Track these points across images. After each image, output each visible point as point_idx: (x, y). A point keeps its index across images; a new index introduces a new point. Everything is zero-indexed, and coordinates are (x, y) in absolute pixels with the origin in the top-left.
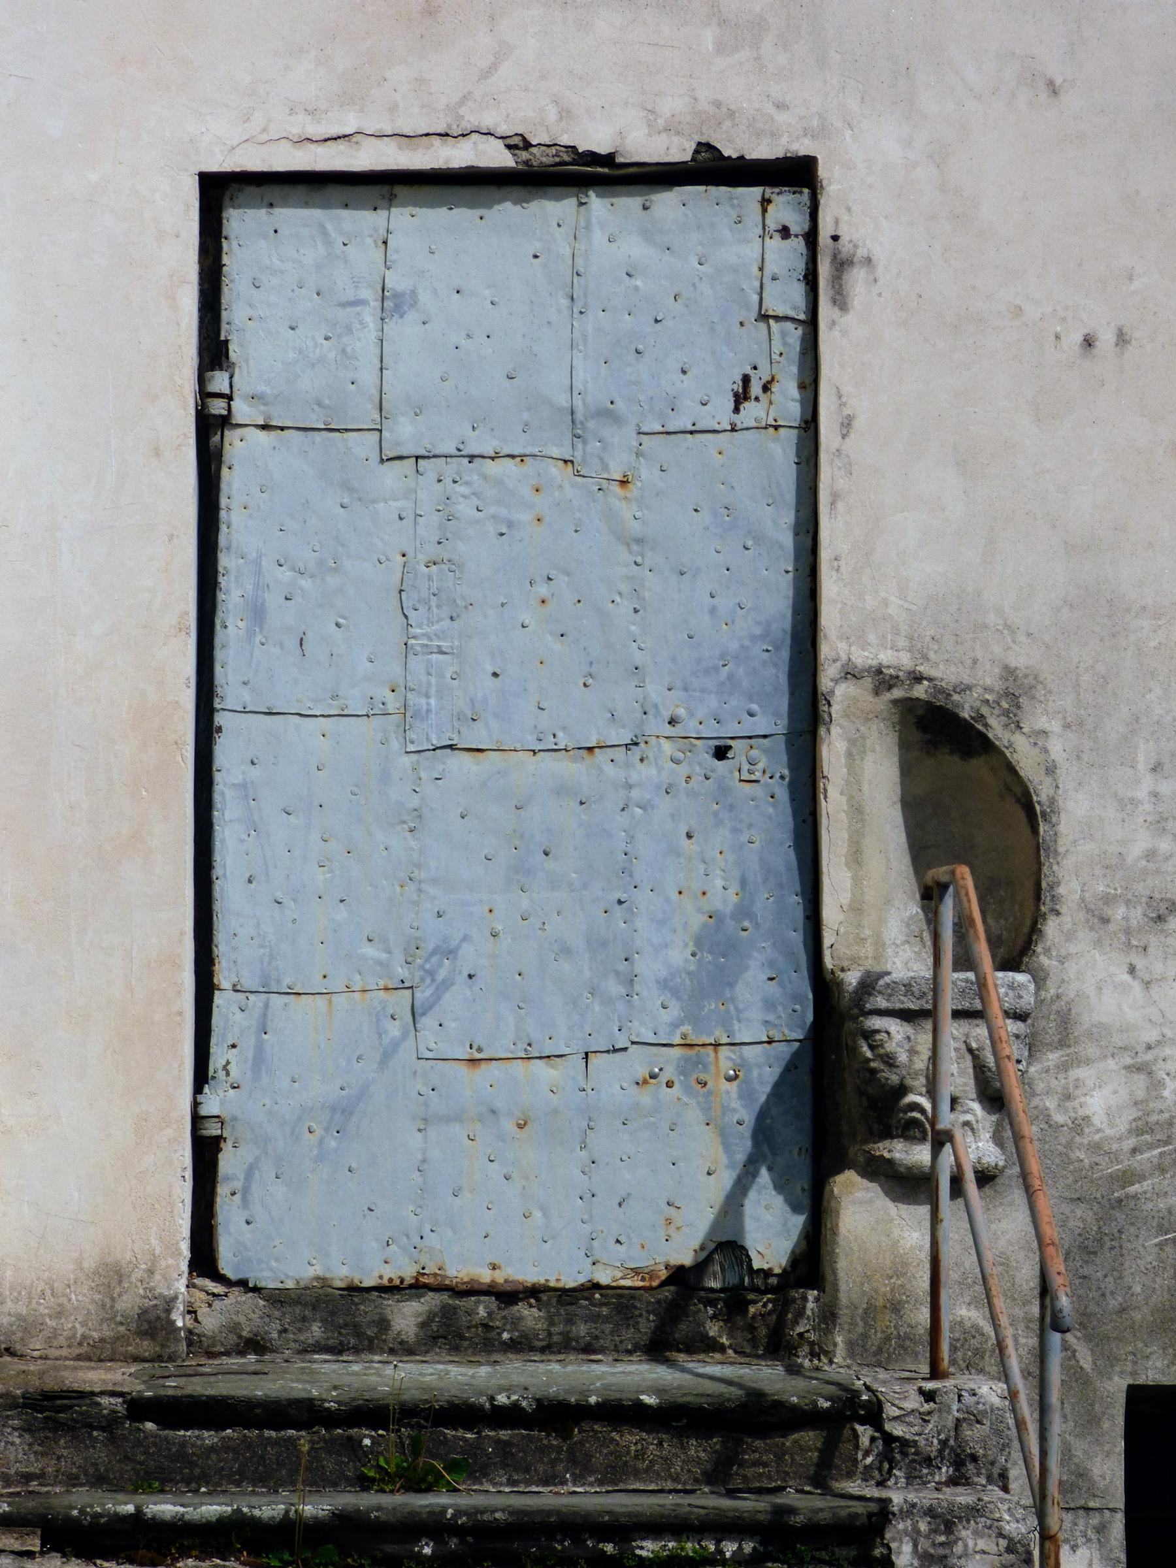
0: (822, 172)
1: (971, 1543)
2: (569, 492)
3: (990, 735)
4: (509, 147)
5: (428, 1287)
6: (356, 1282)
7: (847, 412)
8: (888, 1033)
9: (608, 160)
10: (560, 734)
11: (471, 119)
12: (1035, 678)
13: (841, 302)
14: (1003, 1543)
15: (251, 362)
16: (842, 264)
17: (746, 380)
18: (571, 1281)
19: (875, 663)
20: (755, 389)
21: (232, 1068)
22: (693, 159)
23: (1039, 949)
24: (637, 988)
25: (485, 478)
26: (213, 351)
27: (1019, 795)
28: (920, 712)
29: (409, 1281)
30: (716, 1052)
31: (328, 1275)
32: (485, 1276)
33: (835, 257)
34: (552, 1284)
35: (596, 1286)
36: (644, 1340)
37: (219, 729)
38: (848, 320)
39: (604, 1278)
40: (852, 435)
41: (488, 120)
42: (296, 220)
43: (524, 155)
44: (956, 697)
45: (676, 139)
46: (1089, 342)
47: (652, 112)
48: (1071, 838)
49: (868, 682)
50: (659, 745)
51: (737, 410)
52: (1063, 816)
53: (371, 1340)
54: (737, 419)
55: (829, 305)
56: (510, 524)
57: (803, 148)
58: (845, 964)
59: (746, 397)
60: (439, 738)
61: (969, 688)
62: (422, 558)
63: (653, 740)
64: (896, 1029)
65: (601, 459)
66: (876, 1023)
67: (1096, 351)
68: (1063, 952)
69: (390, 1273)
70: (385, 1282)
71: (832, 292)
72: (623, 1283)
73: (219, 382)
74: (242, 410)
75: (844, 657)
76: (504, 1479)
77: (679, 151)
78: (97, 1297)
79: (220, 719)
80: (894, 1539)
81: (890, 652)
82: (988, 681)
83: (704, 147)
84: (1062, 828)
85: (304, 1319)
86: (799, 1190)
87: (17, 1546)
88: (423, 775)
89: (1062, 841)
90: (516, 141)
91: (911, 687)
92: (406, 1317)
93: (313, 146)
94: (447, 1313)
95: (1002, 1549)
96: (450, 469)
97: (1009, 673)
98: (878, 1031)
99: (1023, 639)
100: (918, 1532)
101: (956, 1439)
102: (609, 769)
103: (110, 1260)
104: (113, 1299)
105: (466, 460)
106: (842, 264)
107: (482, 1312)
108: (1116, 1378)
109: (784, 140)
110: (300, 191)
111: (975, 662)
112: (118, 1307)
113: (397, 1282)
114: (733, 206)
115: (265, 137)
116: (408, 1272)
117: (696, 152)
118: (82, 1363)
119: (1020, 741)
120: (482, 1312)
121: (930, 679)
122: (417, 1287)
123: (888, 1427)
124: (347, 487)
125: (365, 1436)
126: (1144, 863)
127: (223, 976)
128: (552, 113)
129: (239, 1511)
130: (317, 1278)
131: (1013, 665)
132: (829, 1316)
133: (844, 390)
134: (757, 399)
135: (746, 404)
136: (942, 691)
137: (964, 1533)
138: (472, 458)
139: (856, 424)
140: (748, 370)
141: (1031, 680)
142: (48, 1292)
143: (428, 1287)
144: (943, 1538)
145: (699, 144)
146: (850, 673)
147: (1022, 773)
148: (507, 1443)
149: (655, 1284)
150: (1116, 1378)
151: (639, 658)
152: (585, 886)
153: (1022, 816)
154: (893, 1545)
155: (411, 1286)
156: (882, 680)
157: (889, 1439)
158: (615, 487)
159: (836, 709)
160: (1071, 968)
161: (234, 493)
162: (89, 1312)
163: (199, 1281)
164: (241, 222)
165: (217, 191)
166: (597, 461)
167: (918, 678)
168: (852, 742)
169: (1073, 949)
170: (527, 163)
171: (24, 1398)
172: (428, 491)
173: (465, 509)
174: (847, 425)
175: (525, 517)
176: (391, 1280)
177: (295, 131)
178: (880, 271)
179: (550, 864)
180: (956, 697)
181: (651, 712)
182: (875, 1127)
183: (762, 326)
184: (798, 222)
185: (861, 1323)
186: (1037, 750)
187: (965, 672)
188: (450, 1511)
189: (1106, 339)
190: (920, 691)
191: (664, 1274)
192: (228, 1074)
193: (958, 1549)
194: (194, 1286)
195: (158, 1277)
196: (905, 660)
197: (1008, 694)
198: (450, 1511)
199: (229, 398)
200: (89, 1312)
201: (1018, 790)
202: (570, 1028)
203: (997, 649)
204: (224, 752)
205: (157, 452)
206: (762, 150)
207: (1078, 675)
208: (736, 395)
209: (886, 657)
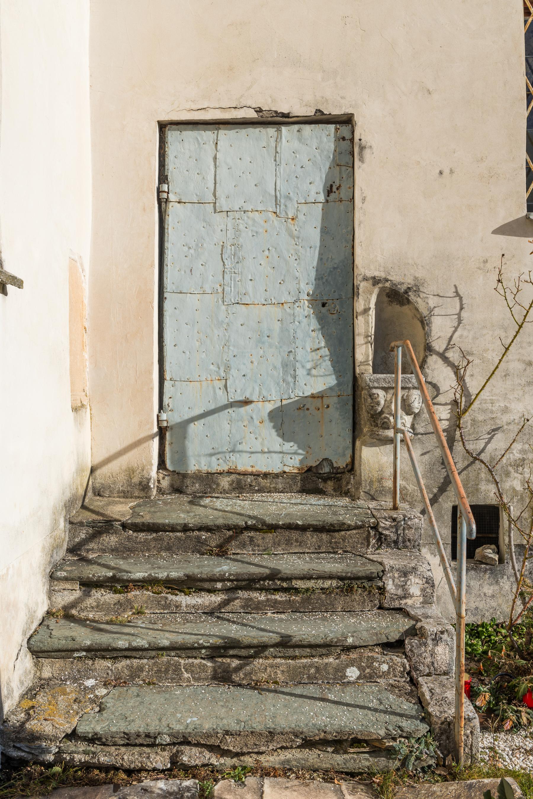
0: (356, 118)
1: (413, 581)
2: (276, 223)
3: (410, 298)
4: (256, 111)
5: (232, 473)
6: (210, 471)
7: (364, 195)
8: (378, 394)
9: (287, 116)
10: (273, 299)
11: (243, 103)
12: (424, 280)
13: (362, 160)
14: (425, 580)
15: (175, 182)
16: (362, 148)
17: (331, 186)
18: (276, 471)
19: (373, 275)
20: (334, 189)
21: (170, 405)
22: (315, 115)
23: (425, 367)
24: (297, 379)
25: (248, 217)
26: (163, 178)
27: (419, 317)
28: (388, 291)
29: (226, 471)
30: (322, 399)
31: (200, 469)
32: (250, 469)
33: (360, 146)
34: (271, 472)
35: (285, 472)
36: (298, 489)
37: (166, 298)
38: (364, 166)
39: (287, 469)
40: (366, 203)
41: (249, 104)
42: (189, 134)
43: (261, 114)
44: (399, 286)
45: (309, 108)
46: (441, 173)
47: (302, 100)
48: (435, 331)
49: (371, 282)
50: (304, 303)
51: (328, 196)
52: (433, 324)
53: (214, 489)
54: (328, 198)
55: (358, 161)
56: (257, 233)
57: (350, 111)
58: (363, 372)
59: (332, 192)
60: (234, 300)
61: (403, 283)
62: (229, 244)
63: (302, 301)
64: (381, 393)
65: (286, 212)
66: (375, 391)
67: (443, 175)
68: (433, 368)
69: (220, 469)
70: (218, 471)
71: (359, 157)
72: (293, 471)
73: (165, 187)
74: (172, 197)
75: (363, 274)
76: (250, 549)
77: (310, 112)
78: (126, 478)
79: (166, 295)
80: (386, 580)
81: (378, 272)
82: (409, 281)
83: (319, 111)
84: (433, 328)
85: (194, 483)
86: (348, 442)
87: (70, 588)
88: (229, 312)
89: (432, 332)
90: (258, 109)
91: (385, 283)
92: (225, 482)
93: (194, 112)
94: (239, 482)
95: (424, 582)
96: (237, 215)
97: (416, 279)
98: (375, 394)
99: (420, 267)
100: (395, 577)
101: (403, 534)
102: (288, 310)
103: (130, 466)
104: (131, 479)
105: (243, 212)
106: (362, 148)
107: (249, 480)
108: (449, 503)
109: (343, 109)
110: (190, 126)
111: (405, 275)
112: (132, 481)
113: (222, 471)
114: (327, 130)
115: (178, 109)
116: (226, 468)
117: (316, 112)
118: (121, 500)
119: (419, 300)
120: (249, 480)
121: (391, 281)
122: (229, 473)
123: (380, 530)
124: (204, 221)
125: (204, 535)
126: (459, 339)
127: (168, 376)
128: (270, 100)
129: (150, 575)
130: (198, 470)
131: (417, 276)
132: (359, 484)
133: (363, 188)
134: (335, 192)
135: (332, 194)
136: (395, 284)
137: (410, 577)
138: (245, 212)
139: (367, 199)
140: (332, 183)
141: (423, 281)
142: (111, 476)
143: (232, 473)
144: (403, 579)
145: (317, 110)
146: (365, 279)
147: (420, 310)
148: (252, 537)
149: (303, 472)
150: (449, 503)
151: (297, 274)
152: (281, 347)
153: (419, 324)
154: (386, 582)
155: (227, 473)
156: (375, 281)
157: (381, 534)
158: (290, 220)
159: (361, 291)
160: (436, 373)
161: (170, 223)
162: (124, 483)
163: (160, 471)
164: (172, 135)
165: (163, 126)
166: (284, 212)
167: (387, 280)
168: (365, 301)
169: (436, 367)
170: (262, 117)
171: (87, 523)
172: (230, 222)
173: (242, 227)
174: (364, 200)
175: (261, 230)
176: (220, 471)
177: (188, 107)
178: (374, 150)
179: (270, 340)
180: (399, 286)
181: (301, 292)
182: (373, 423)
183: (338, 168)
184: (348, 136)
185: (368, 486)
186: (425, 303)
187: (401, 278)
188: (227, 574)
189: (446, 172)
190: (388, 285)
191: (306, 469)
192: (169, 406)
193: (409, 583)
194: (159, 472)
195: (145, 472)
196: (383, 275)
197: (416, 286)
198: (227, 574)
199: (168, 193)
200: (124, 483)
201: (419, 316)
202: (276, 392)
203: (412, 271)
204: (167, 305)
205: (144, 209)
206: (336, 111)
207: (438, 279)
208: (328, 191)
209: (377, 274)
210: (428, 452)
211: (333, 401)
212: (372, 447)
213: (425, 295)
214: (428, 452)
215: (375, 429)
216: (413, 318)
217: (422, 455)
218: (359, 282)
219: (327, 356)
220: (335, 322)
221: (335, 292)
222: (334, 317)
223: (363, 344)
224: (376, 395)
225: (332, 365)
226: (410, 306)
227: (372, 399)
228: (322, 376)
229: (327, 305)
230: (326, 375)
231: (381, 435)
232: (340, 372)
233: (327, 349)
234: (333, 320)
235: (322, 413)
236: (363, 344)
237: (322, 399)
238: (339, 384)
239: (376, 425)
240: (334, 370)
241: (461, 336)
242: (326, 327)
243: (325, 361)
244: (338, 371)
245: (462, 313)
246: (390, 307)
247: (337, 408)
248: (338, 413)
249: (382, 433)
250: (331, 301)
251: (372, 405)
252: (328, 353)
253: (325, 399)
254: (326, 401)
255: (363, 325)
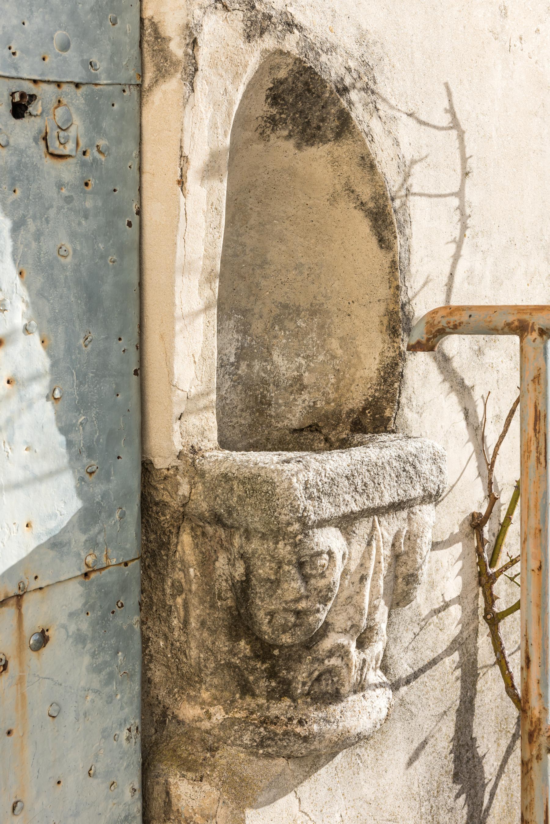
44: (324, 58)
64: (329, 539)
84: (414, 243)
98: (319, 554)
153: (363, 226)
190: (291, 43)
201: (366, 192)
210: (424, 743)
211: (60, 607)
212: (274, 799)
213: (390, 112)
214: (424, 743)
215: (279, 709)
216: (333, 199)
217: (410, 762)
218: (198, 12)
219: (35, 377)
220: (68, 200)
221: (65, 47)
222: (68, 171)
223: (196, 314)
224: (324, 560)
225: (58, 418)
226: (343, 149)
227: (306, 578)
228: (17, 486)
229: (36, 108)
230: (39, 479)
231: (321, 735)
232: (90, 451)
233: (35, 339)
234: (60, 186)
235: (21, 680)
236: (196, 314)
237: (19, 606)
238: (89, 516)
239: (285, 690)
240: (69, 444)
241: (471, 272)
242: (32, 226)
243: (30, 406)
244: (89, 456)
245: (467, 190)
246: (259, 147)
247: (80, 639)
248: (87, 660)
249: (326, 727)
250: (52, 88)
251: (303, 605)
252: (41, 360)
253: (29, 601)
254: (35, 613)
255: (201, 219)
